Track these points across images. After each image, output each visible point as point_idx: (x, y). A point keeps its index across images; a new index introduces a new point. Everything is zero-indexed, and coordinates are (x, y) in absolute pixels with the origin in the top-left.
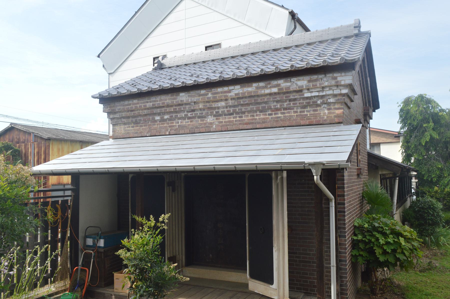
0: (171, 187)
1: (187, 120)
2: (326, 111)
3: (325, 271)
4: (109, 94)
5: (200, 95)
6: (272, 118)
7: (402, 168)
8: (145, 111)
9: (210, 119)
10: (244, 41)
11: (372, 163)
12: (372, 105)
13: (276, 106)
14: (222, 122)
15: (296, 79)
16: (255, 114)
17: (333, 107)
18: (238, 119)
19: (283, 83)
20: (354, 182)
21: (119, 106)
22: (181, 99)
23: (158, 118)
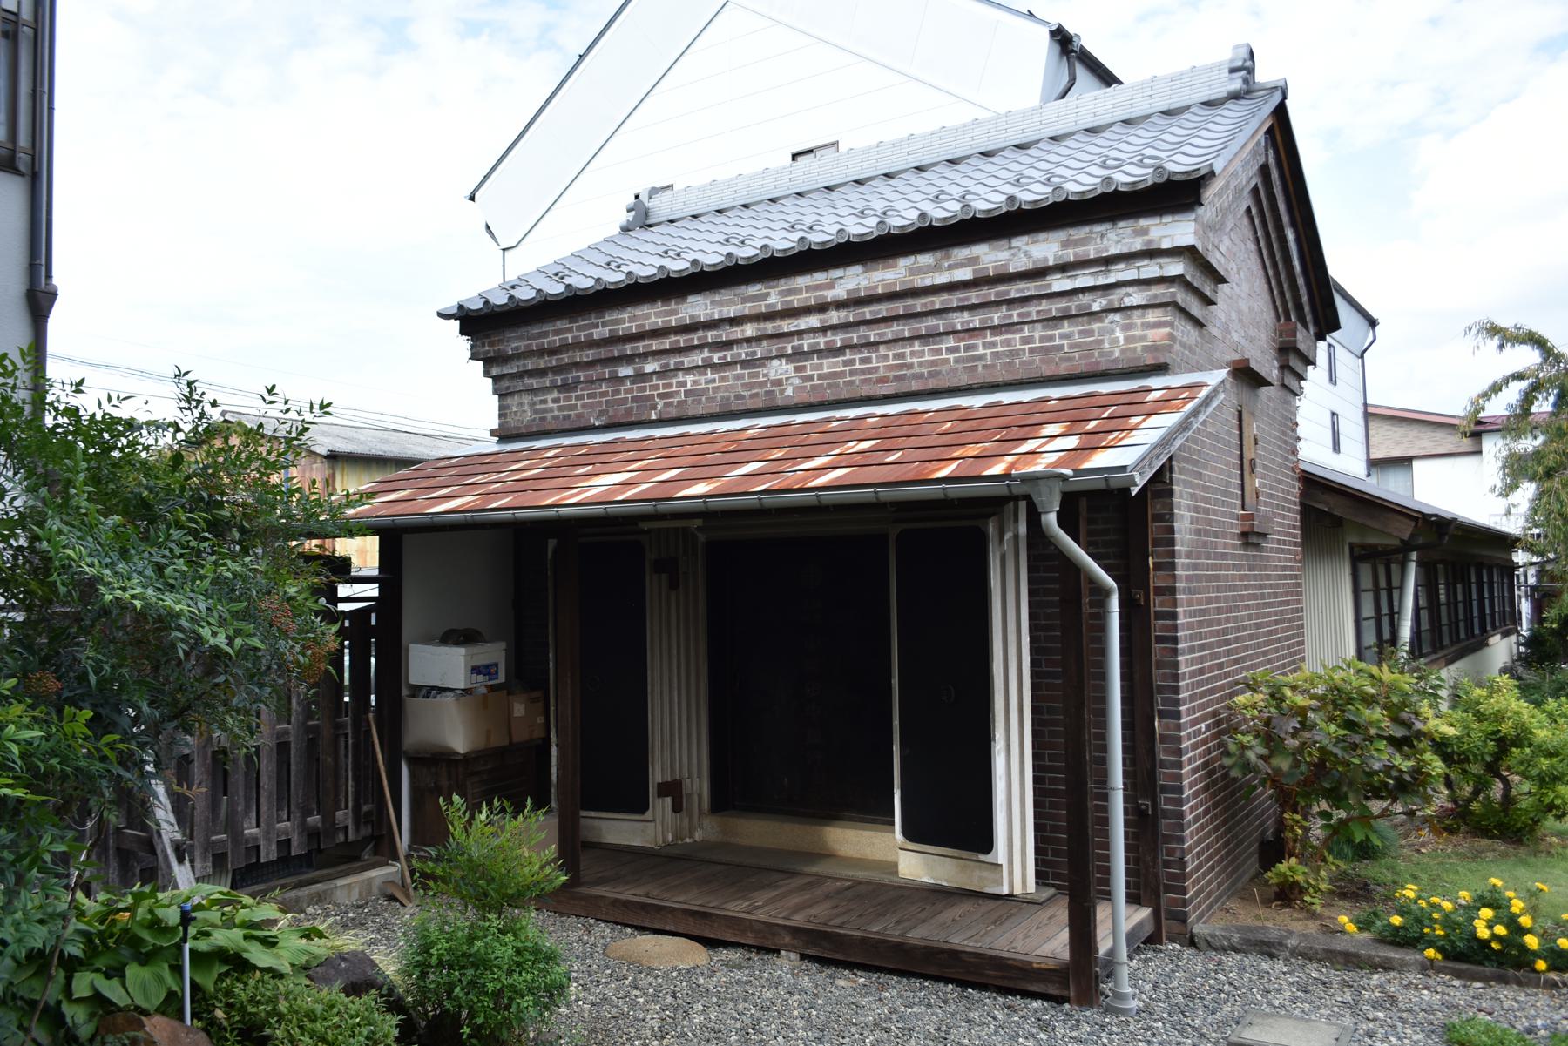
0: (664, 576)
1: (710, 376)
2: (1120, 335)
3: (1089, 805)
4: (487, 303)
5: (745, 300)
6: (957, 361)
7: (1416, 519)
8: (591, 352)
9: (779, 369)
10: (923, 125)
11: (1320, 506)
12: (1309, 317)
13: (968, 322)
14: (811, 378)
15: (1025, 238)
16: (908, 351)
17: (1139, 321)
18: (858, 366)
19: (989, 256)
20: (1224, 556)
21: (515, 342)
22: (692, 312)
23: (625, 371)
